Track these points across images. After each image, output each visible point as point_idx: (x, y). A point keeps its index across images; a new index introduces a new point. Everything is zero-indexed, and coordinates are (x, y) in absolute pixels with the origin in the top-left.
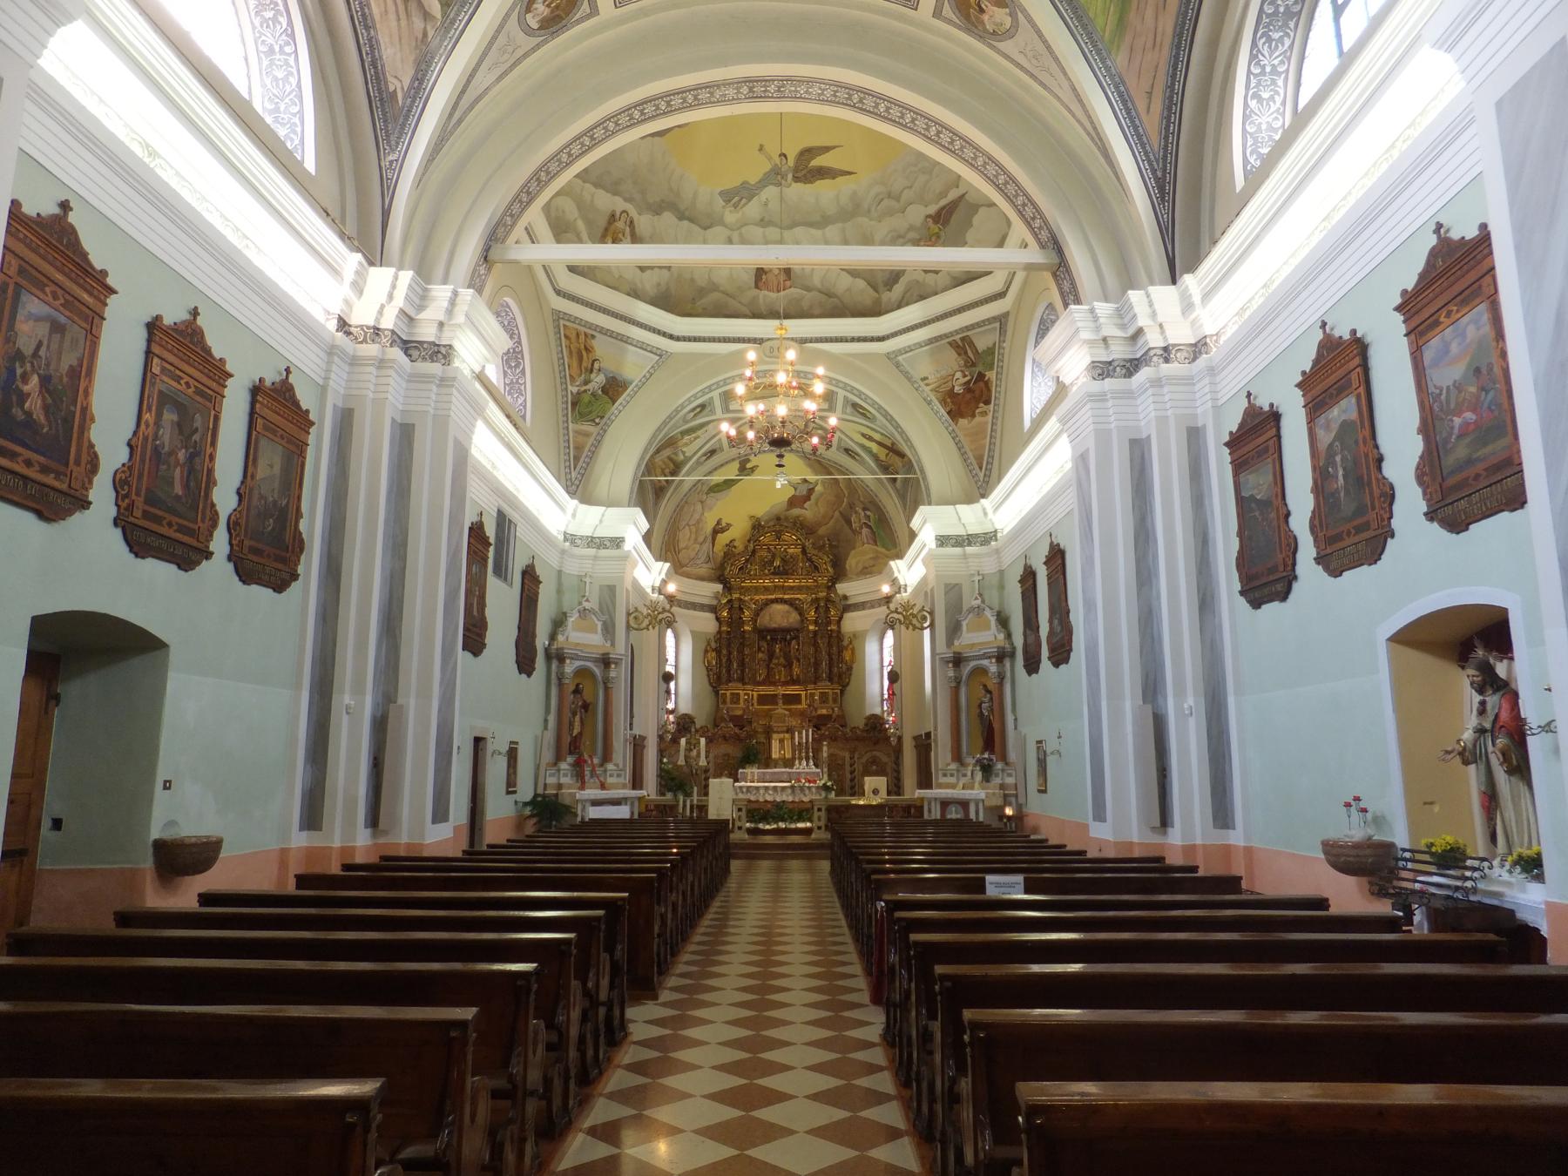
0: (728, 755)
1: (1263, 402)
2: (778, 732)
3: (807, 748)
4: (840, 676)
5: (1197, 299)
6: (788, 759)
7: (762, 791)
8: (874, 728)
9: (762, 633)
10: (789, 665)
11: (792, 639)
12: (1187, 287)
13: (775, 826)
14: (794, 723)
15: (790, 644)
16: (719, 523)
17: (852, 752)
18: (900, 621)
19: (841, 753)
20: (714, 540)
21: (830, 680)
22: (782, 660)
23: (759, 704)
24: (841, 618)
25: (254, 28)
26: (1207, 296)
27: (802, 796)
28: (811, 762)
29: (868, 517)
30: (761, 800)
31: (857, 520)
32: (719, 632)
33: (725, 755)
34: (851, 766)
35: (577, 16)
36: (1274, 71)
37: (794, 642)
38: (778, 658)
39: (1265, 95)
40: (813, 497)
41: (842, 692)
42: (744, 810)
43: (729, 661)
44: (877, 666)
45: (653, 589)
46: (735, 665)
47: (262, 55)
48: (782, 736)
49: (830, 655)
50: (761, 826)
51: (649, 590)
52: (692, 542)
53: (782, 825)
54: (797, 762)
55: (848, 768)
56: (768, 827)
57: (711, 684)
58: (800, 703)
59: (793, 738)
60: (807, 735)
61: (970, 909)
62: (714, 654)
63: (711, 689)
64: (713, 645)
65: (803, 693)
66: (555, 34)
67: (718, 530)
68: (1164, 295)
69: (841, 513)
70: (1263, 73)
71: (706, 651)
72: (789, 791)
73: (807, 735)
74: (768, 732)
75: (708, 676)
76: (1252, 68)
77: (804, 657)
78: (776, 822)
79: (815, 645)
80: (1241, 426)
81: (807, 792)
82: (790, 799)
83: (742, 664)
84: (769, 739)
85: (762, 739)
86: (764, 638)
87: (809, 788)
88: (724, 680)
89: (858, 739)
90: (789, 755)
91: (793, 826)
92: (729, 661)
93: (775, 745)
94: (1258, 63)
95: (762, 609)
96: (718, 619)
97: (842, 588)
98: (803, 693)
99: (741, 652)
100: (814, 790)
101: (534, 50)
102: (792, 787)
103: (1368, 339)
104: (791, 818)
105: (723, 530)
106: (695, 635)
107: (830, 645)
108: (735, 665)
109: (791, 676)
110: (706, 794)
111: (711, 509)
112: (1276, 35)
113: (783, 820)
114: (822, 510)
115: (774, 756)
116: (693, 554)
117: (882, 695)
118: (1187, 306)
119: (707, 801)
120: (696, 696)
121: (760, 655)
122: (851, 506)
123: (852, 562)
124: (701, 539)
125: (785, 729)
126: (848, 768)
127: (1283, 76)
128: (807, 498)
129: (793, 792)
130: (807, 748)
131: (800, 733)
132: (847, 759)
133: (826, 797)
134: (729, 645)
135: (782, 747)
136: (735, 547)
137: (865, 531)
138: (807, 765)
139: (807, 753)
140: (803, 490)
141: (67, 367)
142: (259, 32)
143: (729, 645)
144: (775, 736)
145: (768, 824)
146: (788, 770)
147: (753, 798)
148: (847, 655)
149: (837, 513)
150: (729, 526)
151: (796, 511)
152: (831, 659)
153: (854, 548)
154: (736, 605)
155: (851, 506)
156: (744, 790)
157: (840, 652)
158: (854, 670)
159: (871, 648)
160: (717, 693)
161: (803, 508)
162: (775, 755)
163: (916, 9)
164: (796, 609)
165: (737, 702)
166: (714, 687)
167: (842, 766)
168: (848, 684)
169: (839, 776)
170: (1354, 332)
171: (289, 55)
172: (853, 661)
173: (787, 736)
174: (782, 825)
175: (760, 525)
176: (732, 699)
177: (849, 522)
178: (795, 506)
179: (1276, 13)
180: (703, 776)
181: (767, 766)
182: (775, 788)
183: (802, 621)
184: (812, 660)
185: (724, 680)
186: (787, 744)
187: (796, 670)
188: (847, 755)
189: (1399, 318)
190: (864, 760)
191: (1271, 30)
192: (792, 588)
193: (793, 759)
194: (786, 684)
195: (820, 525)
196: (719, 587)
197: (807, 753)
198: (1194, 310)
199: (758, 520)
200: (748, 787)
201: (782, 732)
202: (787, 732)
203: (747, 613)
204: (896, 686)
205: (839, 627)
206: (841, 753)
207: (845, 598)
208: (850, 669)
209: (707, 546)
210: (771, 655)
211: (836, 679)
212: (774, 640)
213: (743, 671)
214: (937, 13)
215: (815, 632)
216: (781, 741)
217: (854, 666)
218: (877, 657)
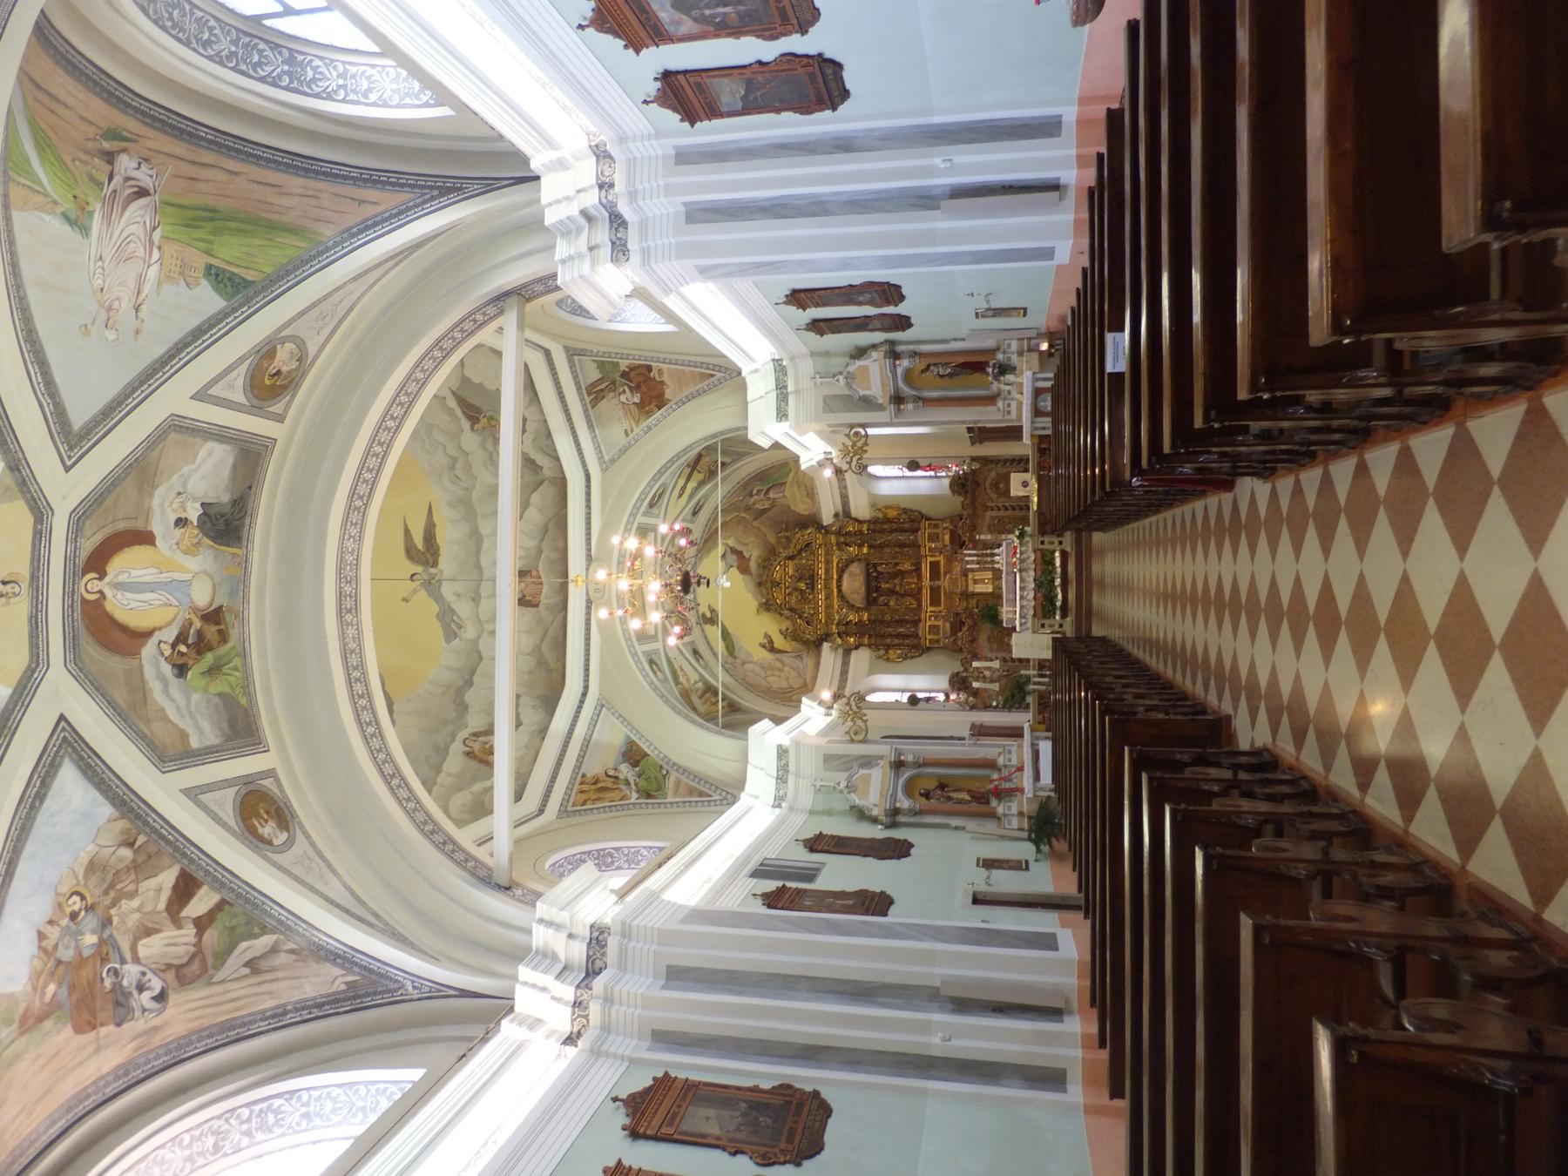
0: (989, 638)
2: (967, 586)
3: (983, 555)
4: (912, 521)
6: (994, 574)
7: (1025, 603)
8: (963, 486)
9: (870, 602)
10: (902, 574)
11: (876, 570)
13: (1059, 590)
14: (959, 568)
15: (881, 573)
16: (763, 646)
17: (987, 508)
18: (859, 459)
19: (988, 520)
20: (780, 651)
21: (916, 531)
22: (896, 581)
23: (939, 605)
24: (856, 520)
25: (283, 1135)
27: (1029, 561)
28: (996, 551)
29: (759, 492)
30: (1033, 603)
31: (762, 503)
32: (870, 646)
33: (989, 641)
34: (999, 510)
35: (278, 793)
37: (879, 569)
38: (895, 586)
40: (739, 549)
41: (928, 519)
42: (1043, 622)
43: (897, 636)
44: (902, 483)
45: (827, 715)
46: (901, 630)
48: (970, 582)
49: (892, 532)
50: (1059, 604)
51: (829, 719)
52: (781, 674)
53: (1058, 581)
54: (996, 566)
55: (1002, 513)
56: (1060, 597)
57: (920, 655)
58: (938, 562)
59: (973, 570)
60: (970, 555)
62: (891, 652)
63: (924, 656)
64: (882, 652)
65: (929, 559)
67: (772, 649)
69: (755, 519)
70: (344, 87)
71: (888, 660)
72: (1024, 574)
73: (970, 555)
74: (967, 595)
75: (912, 657)
77: (894, 558)
78: (1055, 588)
79: (881, 546)
80: (675, 110)
81: (1025, 556)
82: (1032, 573)
83: (901, 622)
84: (974, 595)
85: (973, 602)
86: (875, 599)
87: (1021, 553)
88: (916, 642)
89: (973, 502)
90: (989, 575)
91: (1059, 570)
92: (897, 636)
93: (980, 588)
95: (848, 602)
96: (857, 648)
97: (827, 519)
98: (929, 559)
99: (889, 624)
100: (1023, 549)
101: (308, 837)
102: (1021, 571)
104: (1051, 572)
105: (771, 642)
106: (872, 672)
107: (882, 531)
108: (901, 630)
109: (912, 571)
110: (1028, 660)
111: (750, 655)
113: (1053, 581)
114: (751, 539)
115: (990, 590)
116: (794, 674)
117: (931, 477)
119: (1034, 660)
120: (932, 670)
121: (892, 603)
122: (748, 509)
123: (802, 508)
124: (779, 665)
125: (964, 578)
126: (1002, 513)
128: (739, 554)
129: (1025, 570)
130: (983, 555)
131: (968, 562)
132: (994, 513)
133: (1031, 536)
134: (883, 636)
135: (982, 581)
136: (787, 630)
137: (772, 495)
138: (998, 555)
139: (987, 555)
140: (733, 558)
143: (883, 636)
144: (971, 589)
145: (1056, 596)
146: (1004, 576)
147: (1032, 613)
148: (892, 514)
149: (755, 524)
150: (766, 636)
151: (753, 566)
152: (896, 530)
153: (789, 506)
154: (843, 628)
155: (748, 509)
156: (1023, 621)
157: (890, 521)
158: (908, 507)
159: (885, 489)
160: (929, 649)
161: (749, 559)
162: (989, 589)
163: (276, 440)
164: (847, 566)
165: (937, 627)
166: (923, 652)
167: (1000, 519)
168: (920, 513)
169: (1009, 523)
172: (899, 508)
173: (970, 576)
174: (1058, 581)
175: (766, 603)
176: (935, 634)
177: (764, 511)
178: (748, 566)
179: (289, 73)
180: (1010, 663)
181: (1000, 597)
182: (1021, 589)
183: (859, 560)
184: (897, 549)
185: (916, 642)
186: (978, 576)
187: (907, 566)
188: (989, 514)
190: (994, 496)
192: (827, 571)
193: (993, 570)
194: (920, 578)
195: (766, 542)
196: (826, 646)
197: (987, 555)
199: (761, 605)
200: (1021, 617)
201: (967, 581)
202: (967, 576)
203: (851, 617)
204: (922, 463)
205: (864, 522)
206: (988, 520)
207: (836, 515)
208: (905, 511)
209: (784, 657)
210: (892, 592)
211: (915, 525)
212: (877, 589)
213: (907, 622)
214: (280, 418)
215: (870, 547)
216: (976, 582)
217: (903, 506)
218: (895, 483)
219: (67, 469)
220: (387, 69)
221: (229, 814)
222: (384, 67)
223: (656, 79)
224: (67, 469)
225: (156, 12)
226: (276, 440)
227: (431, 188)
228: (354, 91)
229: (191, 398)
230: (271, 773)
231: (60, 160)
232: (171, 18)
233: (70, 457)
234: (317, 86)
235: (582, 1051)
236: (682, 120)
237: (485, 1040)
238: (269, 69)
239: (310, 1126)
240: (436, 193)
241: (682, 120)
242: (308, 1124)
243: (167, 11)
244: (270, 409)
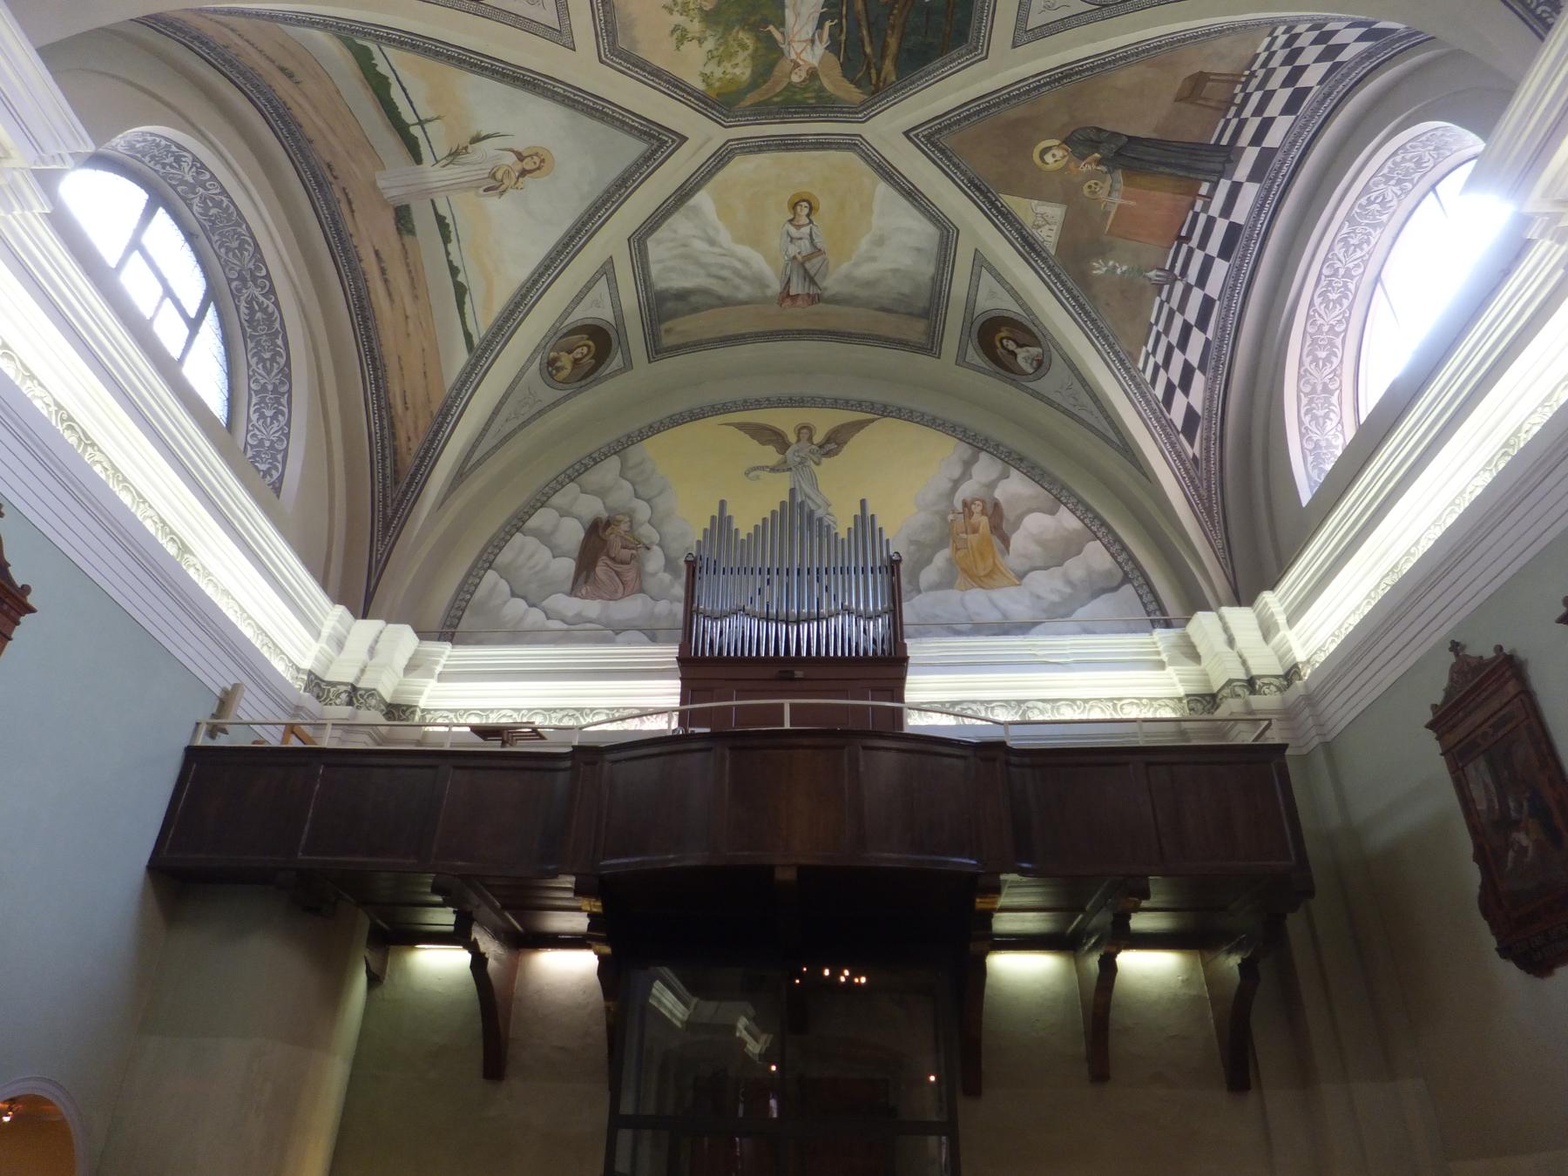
1: (1482, 648)
5: (1281, 619)
12: (1266, 604)
25: (249, 366)
26: (1293, 618)
35: (607, 372)
36: (1325, 389)
39: (1321, 413)
47: (253, 392)
61: (1327, 562)
66: (581, 389)
68: (1240, 618)
70: (1314, 391)
76: (1301, 386)
80: (1449, 693)
94: (1331, 266)
101: (555, 404)
103: (1521, 655)
112: (1322, 354)
118: (1267, 630)
127: (1337, 393)
141: (1152, 889)
142: (253, 370)
163: (939, 358)
170: (1499, 649)
171: (283, 394)
179: (1314, 391)
189: (1431, 735)
191: (1330, 291)
198: (1279, 631)
214: (961, 360)
219: (906, 134)
220: (1340, 436)
221: (581, 314)
222: (1342, 432)
223: (1499, 649)
224: (906, 134)
225: (1357, 266)
226: (939, 358)
227: (1209, 489)
228: (1311, 401)
229: (976, 250)
230: (628, 365)
231: (1200, 732)
232: (1370, 202)
233: (916, 136)
234: (1321, 304)
235: (300, 697)
236: (1434, 707)
237: (324, 585)
238: (1322, 309)
239: (253, 392)
240: (1204, 493)
241: (1434, 707)
242: (255, 391)
243: (1376, 198)
244: (970, 346)
